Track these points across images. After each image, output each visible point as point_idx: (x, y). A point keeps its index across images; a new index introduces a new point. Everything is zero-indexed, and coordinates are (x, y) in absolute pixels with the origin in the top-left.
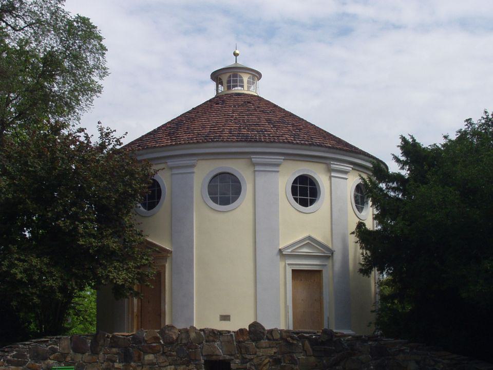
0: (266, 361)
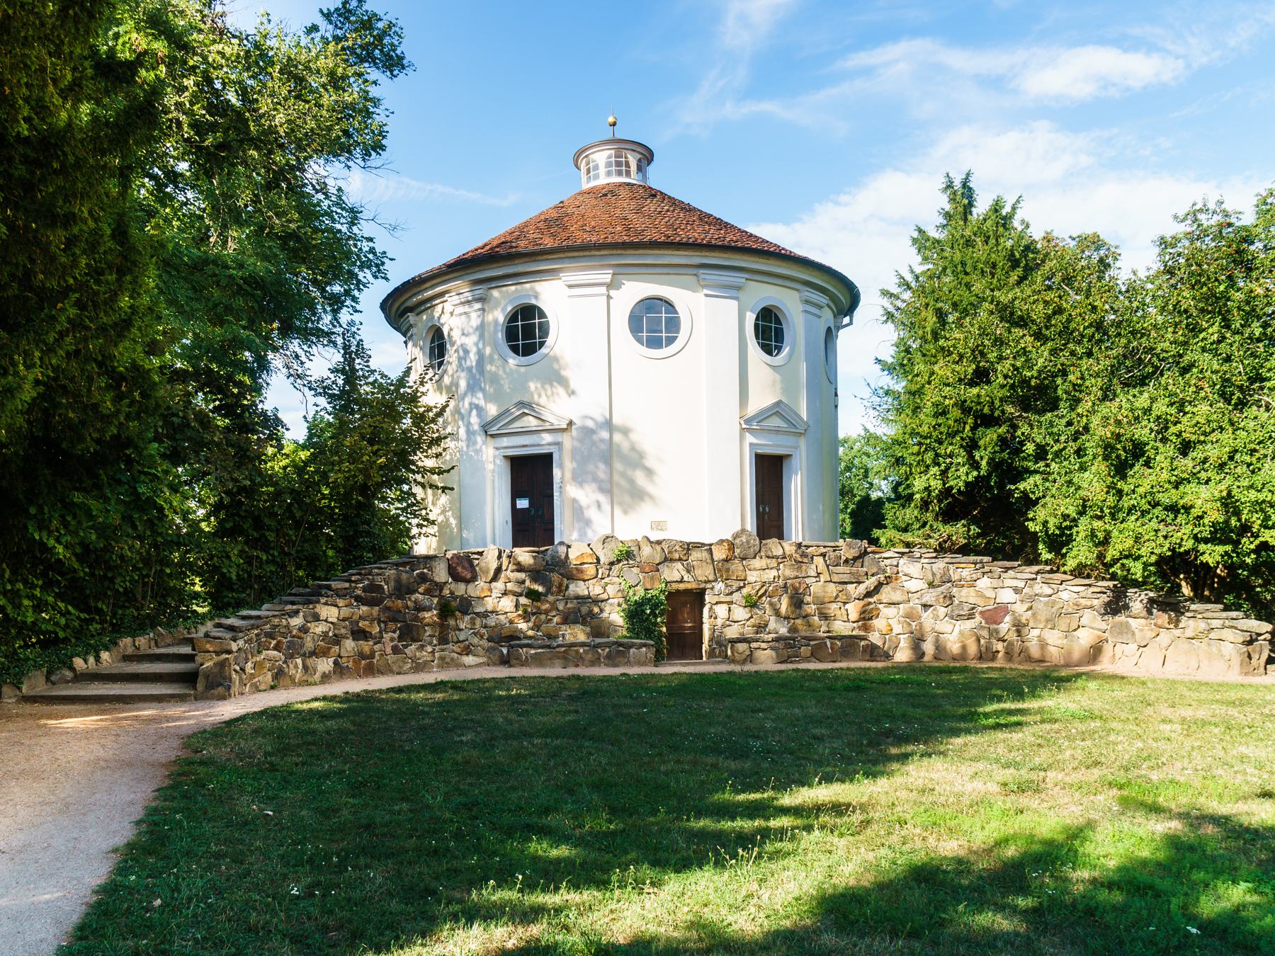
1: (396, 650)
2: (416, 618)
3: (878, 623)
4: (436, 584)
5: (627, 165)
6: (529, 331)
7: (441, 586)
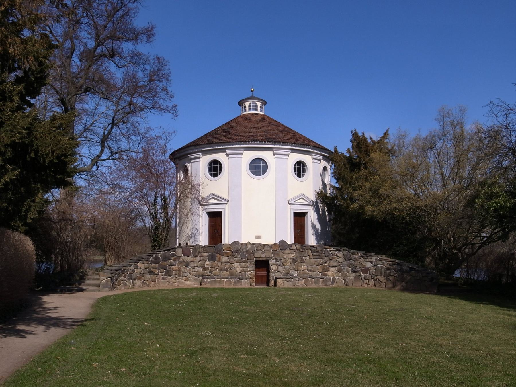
0: (288, 261)
1: (163, 279)
2: (170, 268)
3: (329, 273)
4: (178, 257)
5: (257, 106)
6: (258, 167)
7: (179, 258)
